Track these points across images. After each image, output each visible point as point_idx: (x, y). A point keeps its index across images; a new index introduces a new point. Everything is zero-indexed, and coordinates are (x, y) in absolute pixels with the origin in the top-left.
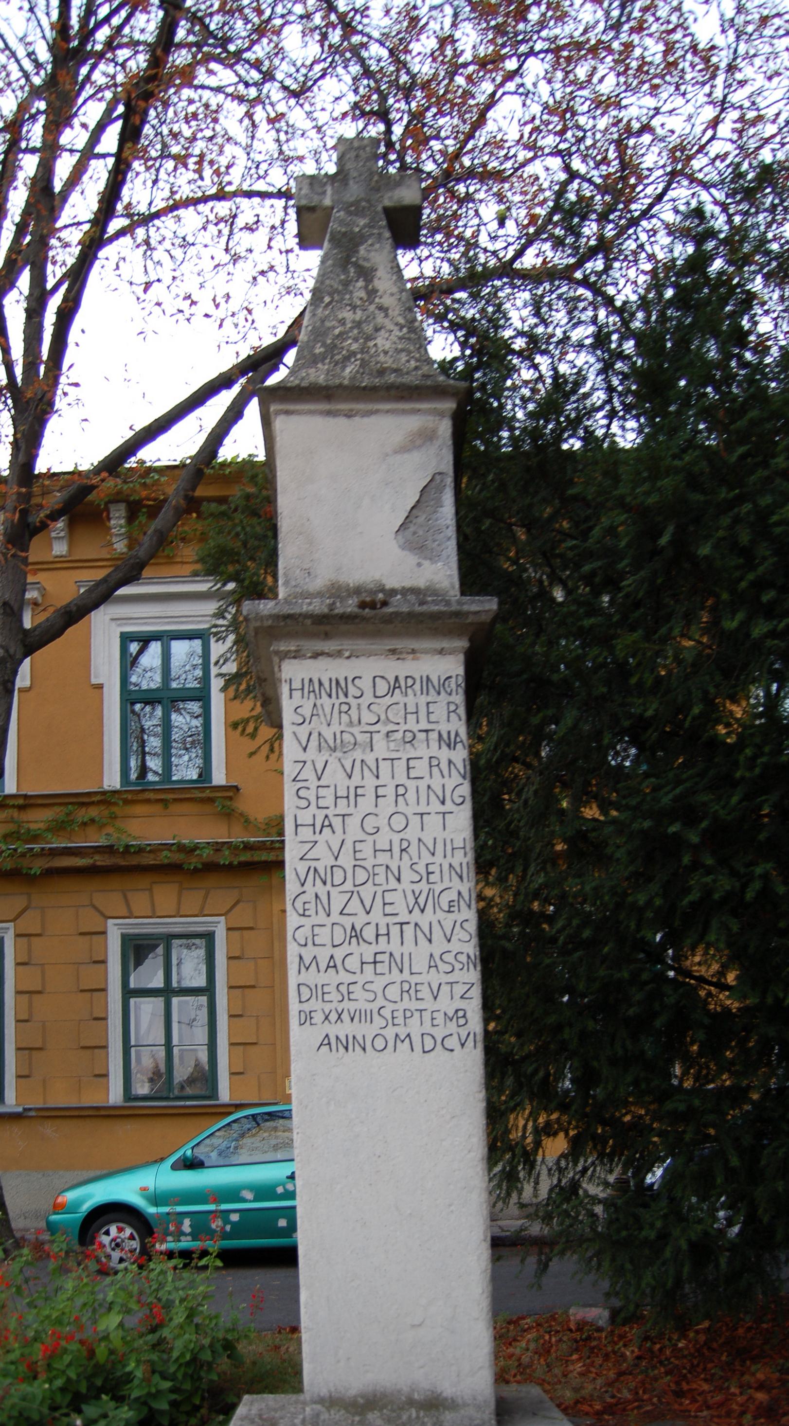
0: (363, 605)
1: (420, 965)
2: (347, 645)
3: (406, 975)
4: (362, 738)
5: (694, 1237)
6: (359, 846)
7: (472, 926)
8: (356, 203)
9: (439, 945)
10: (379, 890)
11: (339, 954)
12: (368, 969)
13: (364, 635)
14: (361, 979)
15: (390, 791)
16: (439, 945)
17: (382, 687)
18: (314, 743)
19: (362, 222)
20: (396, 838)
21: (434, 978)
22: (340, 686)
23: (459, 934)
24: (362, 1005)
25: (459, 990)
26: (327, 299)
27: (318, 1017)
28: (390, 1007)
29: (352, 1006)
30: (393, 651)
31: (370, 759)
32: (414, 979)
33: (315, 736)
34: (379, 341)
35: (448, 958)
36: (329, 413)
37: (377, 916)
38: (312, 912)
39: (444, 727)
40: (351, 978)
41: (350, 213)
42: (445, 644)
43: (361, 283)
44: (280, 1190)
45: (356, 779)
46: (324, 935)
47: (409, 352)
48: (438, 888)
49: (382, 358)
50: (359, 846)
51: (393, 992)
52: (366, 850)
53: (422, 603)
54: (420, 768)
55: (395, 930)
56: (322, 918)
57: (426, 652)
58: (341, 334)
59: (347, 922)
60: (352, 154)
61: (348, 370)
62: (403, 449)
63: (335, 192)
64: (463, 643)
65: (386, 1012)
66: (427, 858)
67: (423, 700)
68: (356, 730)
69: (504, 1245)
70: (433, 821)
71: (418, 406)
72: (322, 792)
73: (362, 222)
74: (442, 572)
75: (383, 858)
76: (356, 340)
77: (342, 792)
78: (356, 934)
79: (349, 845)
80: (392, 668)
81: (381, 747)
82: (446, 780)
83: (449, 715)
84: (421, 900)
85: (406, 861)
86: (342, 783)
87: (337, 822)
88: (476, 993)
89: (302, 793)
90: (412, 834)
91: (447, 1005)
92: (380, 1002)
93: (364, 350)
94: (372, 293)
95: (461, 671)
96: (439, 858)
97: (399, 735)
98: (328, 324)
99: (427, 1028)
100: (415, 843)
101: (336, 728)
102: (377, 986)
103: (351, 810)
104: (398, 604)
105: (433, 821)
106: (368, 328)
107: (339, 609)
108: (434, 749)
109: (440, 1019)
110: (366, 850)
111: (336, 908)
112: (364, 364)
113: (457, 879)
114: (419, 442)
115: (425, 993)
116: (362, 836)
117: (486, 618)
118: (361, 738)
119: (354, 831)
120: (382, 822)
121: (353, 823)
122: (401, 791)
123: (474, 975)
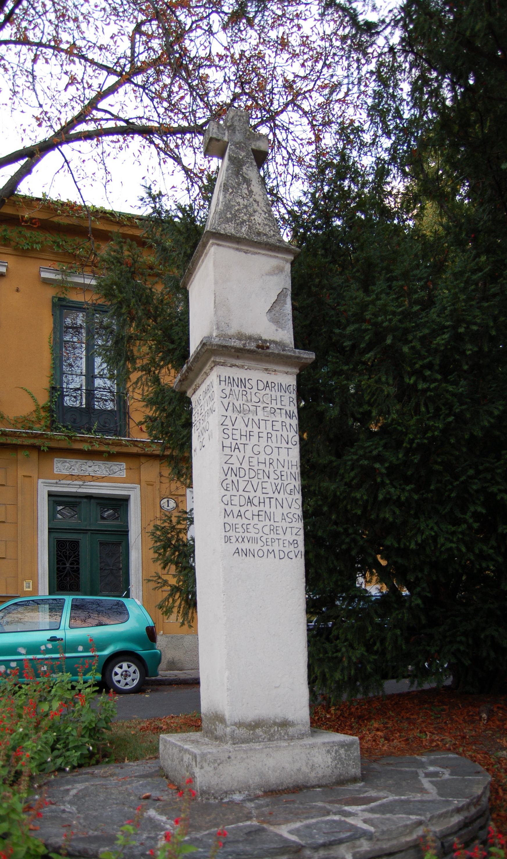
0: (258, 347)
1: (278, 518)
2: (247, 363)
3: (272, 522)
4: (252, 408)
5: (358, 656)
6: (251, 460)
7: (300, 502)
8: (239, 143)
9: (286, 510)
10: (260, 481)
11: (243, 510)
12: (256, 518)
13: (254, 360)
14: (252, 523)
15: (264, 435)
16: (286, 510)
17: (261, 386)
18: (231, 408)
19: (243, 154)
20: (268, 458)
21: (285, 525)
22: (242, 382)
23: (295, 505)
24: (253, 535)
25: (295, 531)
26: (230, 190)
27: (233, 539)
28: (265, 537)
29: (249, 535)
30: (266, 370)
31: (256, 419)
32: (276, 524)
33: (231, 404)
34: (256, 217)
35: (290, 515)
36: (237, 249)
37: (259, 493)
38: (230, 489)
39: (288, 408)
40: (247, 522)
41: (237, 148)
42: (289, 370)
43: (245, 186)
44: (43, 648)
45: (250, 428)
46: (236, 501)
47: (270, 227)
48: (286, 483)
49: (258, 226)
50: (251, 460)
51: (267, 530)
52: (254, 461)
53: (283, 350)
54: (278, 426)
55: (267, 501)
56: (235, 492)
57: (280, 372)
58: (238, 210)
59: (246, 495)
60: (238, 118)
61: (243, 229)
62: (271, 273)
63: (229, 135)
64: (297, 371)
65: (263, 539)
66: (281, 468)
67: (279, 394)
68: (249, 404)
69: (164, 685)
70: (283, 451)
71: (280, 255)
72: (235, 432)
73: (243, 154)
74: (285, 335)
75: (262, 466)
76: (246, 215)
77: (244, 433)
78: (250, 501)
79: (246, 458)
80: (266, 377)
81: (261, 414)
82: (289, 433)
83: (289, 403)
84: (278, 488)
85: (272, 470)
86: (244, 429)
87: (241, 447)
88: (302, 532)
89: (225, 431)
90: (274, 456)
91: (289, 537)
92: (261, 534)
93: (249, 220)
94: (251, 192)
95: (295, 383)
96: (286, 469)
97: (268, 409)
98: (232, 203)
99: (281, 548)
100: (275, 461)
101: (241, 402)
102: (260, 526)
103: (248, 442)
104: (273, 349)
105: (283, 451)
106: (251, 210)
107: (248, 347)
108: (284, 418)
109: (287, 544)
110: (254, 461)
111: (241, 488)
112: (250, 228)
113: (293, 479)
114: (276, 272)
115: (280, 531)
116: (253, 455)
117: (310, 362)
118: (252, 408)
119: (249, 453)
120: (261, 449)
121: (249, 448)
122: (269, 435)
123: (300, 525)
